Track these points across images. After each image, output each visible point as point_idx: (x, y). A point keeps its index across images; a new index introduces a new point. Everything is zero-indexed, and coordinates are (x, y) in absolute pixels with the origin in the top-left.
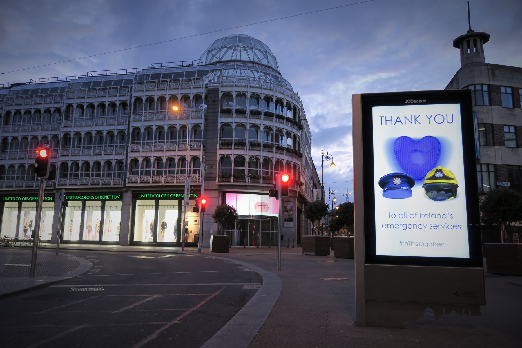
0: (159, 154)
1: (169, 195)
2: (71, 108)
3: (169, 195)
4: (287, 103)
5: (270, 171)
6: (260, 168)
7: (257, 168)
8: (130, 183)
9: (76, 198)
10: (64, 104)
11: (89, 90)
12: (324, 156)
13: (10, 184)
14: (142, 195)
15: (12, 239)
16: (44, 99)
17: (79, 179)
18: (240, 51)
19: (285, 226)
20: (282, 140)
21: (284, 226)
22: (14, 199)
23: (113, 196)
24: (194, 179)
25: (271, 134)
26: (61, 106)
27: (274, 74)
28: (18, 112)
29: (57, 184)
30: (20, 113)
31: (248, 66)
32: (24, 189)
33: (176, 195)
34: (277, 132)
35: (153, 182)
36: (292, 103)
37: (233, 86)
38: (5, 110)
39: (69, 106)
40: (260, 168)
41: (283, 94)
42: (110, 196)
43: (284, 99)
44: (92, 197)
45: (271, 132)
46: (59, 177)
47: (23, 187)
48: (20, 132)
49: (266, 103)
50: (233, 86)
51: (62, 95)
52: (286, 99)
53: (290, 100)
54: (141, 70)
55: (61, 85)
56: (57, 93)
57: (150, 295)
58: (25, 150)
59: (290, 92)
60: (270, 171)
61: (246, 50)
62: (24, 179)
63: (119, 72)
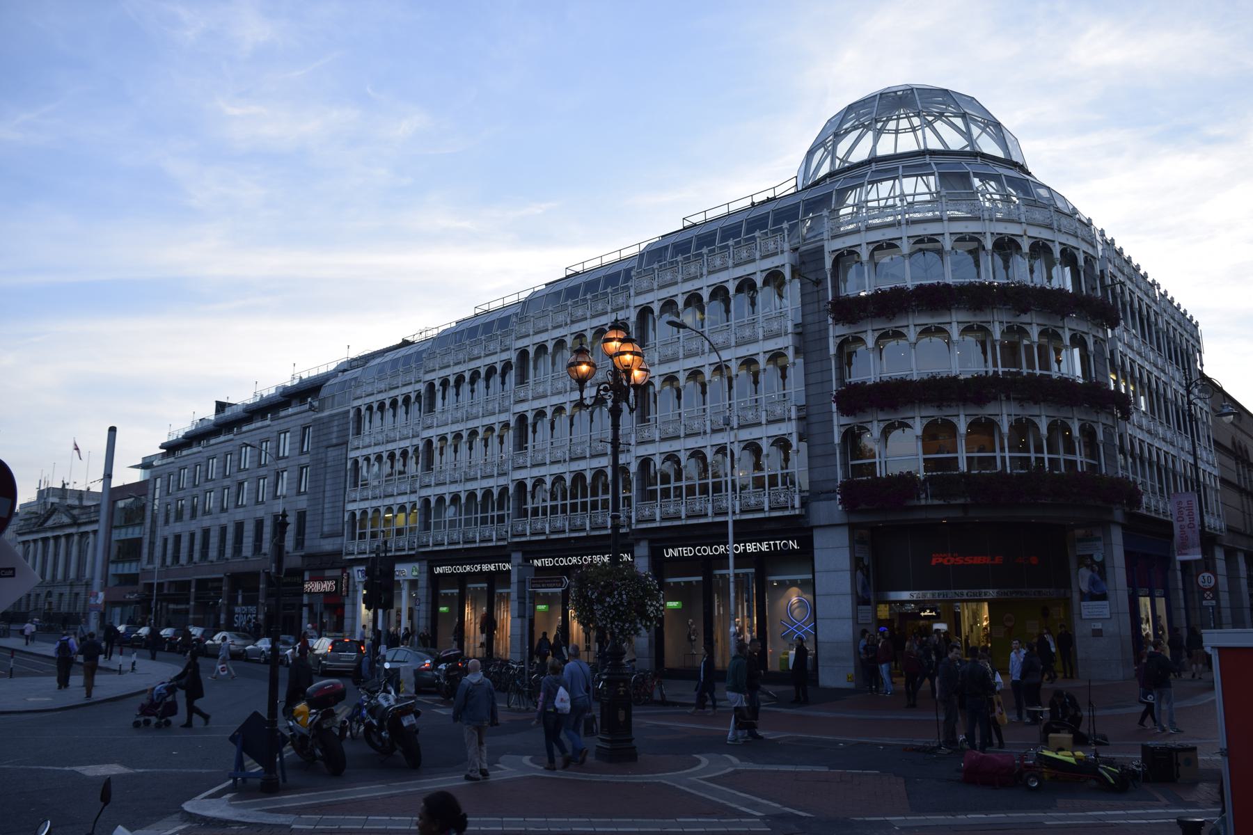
0: (751, 434)
1: (581, 559)
2: (650, 316)
3: (581, 559)
4: (1063, 252)
5: (1033, 455)
6: (1002, 449)
7: (994, 451)
8: (641, 521)
9: (687, 553)
10: (632, 309)
11: (767, 235)
12: (1194, 385)
13: (672, 510)
14: (670, 550)
15: (315, 650)
16: (758, 247)
17: (711, 500)
18: (897, 132)
19: (1083, 617)
20: (1059, 362)
21: (1081, 614)
22: (691, 552)
23: (778, 542)
24: (782, 499)
25: (1026, 346)
26: (783, 263)
27: (1014, 173)
28: (541, 348)
29: (633, 521)
30: (700, 298)
31: (936, 164)
32: (710, 520)
33: (745, 546)
34: (1044, 341)
35: (663, 519)
36: (1078, 249)
37: (940, 220)
38: (425, 382)
39: (645, 312)
40: (1002, 449)
41: (1049, 227)
42: (772, 543)
43: (1053, 241)
44: (578, 561)
45: (1026, 342)
46: (637, 502)
47: (706, 515)
48: (761, 342)
49: (999, 261)
50: (940, 220)
51: (628, 288)
52: (1058, 241)
53: (1072, 242)
54: (454, 325)
55: (627, 264)
56: (767, 228)
57: (704, 782)
58: (721, 400)
59: (1069, 219)
60: (1033, 455)
61: (930, 124)
62: (681, 496)
63: (606, 260)
